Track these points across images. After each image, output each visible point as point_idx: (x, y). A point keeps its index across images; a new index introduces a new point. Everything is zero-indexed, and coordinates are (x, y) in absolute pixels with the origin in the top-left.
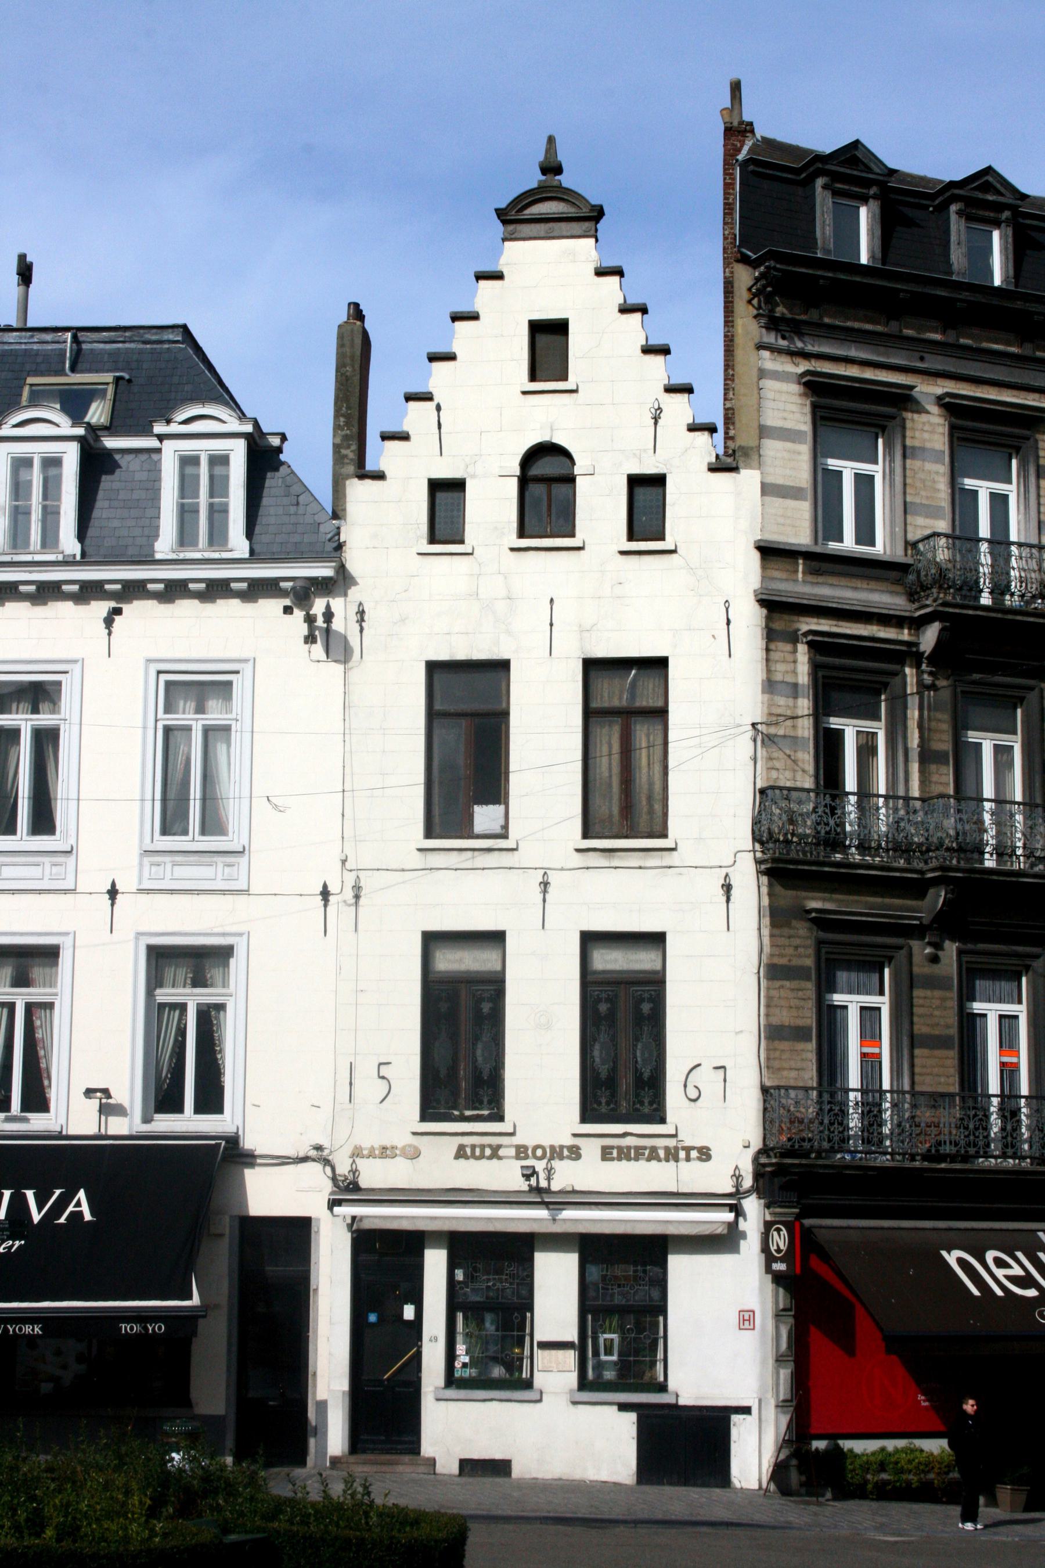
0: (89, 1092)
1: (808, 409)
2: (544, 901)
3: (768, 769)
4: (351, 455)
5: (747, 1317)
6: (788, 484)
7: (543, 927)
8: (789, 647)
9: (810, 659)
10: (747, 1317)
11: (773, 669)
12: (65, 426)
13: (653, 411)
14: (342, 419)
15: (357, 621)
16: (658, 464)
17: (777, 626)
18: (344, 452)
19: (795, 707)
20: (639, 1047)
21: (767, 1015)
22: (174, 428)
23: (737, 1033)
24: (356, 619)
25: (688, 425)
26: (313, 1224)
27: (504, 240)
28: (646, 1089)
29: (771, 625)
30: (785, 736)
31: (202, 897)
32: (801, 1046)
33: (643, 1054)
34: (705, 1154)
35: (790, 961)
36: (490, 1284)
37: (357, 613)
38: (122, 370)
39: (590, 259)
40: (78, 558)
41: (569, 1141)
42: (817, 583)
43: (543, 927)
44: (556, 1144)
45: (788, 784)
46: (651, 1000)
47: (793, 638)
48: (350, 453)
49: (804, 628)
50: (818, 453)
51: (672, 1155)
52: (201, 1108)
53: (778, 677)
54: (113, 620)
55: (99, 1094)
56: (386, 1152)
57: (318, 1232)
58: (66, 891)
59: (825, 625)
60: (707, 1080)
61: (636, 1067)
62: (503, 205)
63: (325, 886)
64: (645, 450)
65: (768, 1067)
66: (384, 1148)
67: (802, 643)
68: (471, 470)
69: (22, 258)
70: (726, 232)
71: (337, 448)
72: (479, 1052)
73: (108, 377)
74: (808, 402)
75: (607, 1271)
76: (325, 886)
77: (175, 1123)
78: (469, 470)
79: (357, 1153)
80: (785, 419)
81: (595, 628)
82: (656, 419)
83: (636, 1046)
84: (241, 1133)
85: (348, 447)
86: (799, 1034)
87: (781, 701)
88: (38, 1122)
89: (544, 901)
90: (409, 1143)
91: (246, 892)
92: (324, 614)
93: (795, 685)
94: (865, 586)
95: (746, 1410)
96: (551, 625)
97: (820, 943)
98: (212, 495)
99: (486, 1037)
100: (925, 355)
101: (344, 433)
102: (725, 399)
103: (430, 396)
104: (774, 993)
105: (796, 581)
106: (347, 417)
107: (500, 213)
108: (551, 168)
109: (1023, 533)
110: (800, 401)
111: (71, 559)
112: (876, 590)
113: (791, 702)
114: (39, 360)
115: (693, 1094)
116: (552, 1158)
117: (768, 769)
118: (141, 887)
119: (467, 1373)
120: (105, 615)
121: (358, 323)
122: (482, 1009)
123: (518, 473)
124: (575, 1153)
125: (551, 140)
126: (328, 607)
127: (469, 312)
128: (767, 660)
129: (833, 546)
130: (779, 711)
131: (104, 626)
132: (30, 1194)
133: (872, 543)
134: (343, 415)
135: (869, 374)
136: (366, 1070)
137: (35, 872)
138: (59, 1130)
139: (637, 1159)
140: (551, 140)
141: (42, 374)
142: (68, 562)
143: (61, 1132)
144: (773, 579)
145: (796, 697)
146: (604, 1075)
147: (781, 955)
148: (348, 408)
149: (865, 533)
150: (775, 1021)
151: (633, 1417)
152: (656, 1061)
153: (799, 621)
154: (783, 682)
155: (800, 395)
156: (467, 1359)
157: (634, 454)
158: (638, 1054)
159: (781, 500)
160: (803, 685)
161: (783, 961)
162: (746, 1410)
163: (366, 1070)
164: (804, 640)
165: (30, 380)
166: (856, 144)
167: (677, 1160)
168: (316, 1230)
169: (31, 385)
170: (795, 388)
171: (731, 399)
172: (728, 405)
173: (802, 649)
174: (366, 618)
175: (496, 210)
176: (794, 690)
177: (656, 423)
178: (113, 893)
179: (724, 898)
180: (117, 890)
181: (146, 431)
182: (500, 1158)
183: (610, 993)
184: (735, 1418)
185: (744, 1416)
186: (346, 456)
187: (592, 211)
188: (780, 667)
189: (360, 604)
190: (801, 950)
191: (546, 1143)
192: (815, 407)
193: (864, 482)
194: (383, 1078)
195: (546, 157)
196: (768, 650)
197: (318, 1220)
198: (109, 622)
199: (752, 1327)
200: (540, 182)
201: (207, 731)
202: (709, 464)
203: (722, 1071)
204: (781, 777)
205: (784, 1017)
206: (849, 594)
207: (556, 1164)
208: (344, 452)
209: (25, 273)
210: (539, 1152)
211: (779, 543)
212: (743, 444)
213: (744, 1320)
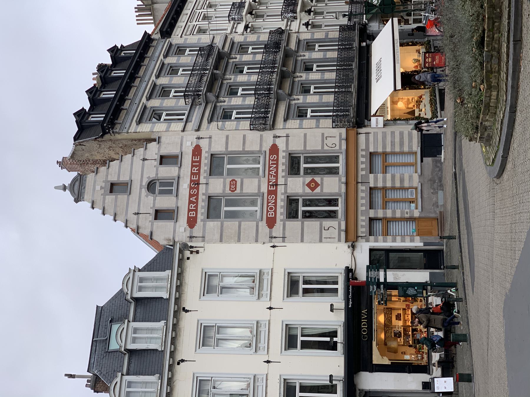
22: (129, 292)
33: (322, 161)
40: (166, 321)
52: (336, 283)
57: (374, 247)
58: (269, 323)
97: (293, 119)
100: (125, 127)
107: (77, 201)
109: (156, 250)
120: (184, 312)
132: (362, 318)
137: (260, 388)
146: (328, 203)
151: (424, 159)
178: (268, 362)
197: (370, 246)
198: (187, 311)
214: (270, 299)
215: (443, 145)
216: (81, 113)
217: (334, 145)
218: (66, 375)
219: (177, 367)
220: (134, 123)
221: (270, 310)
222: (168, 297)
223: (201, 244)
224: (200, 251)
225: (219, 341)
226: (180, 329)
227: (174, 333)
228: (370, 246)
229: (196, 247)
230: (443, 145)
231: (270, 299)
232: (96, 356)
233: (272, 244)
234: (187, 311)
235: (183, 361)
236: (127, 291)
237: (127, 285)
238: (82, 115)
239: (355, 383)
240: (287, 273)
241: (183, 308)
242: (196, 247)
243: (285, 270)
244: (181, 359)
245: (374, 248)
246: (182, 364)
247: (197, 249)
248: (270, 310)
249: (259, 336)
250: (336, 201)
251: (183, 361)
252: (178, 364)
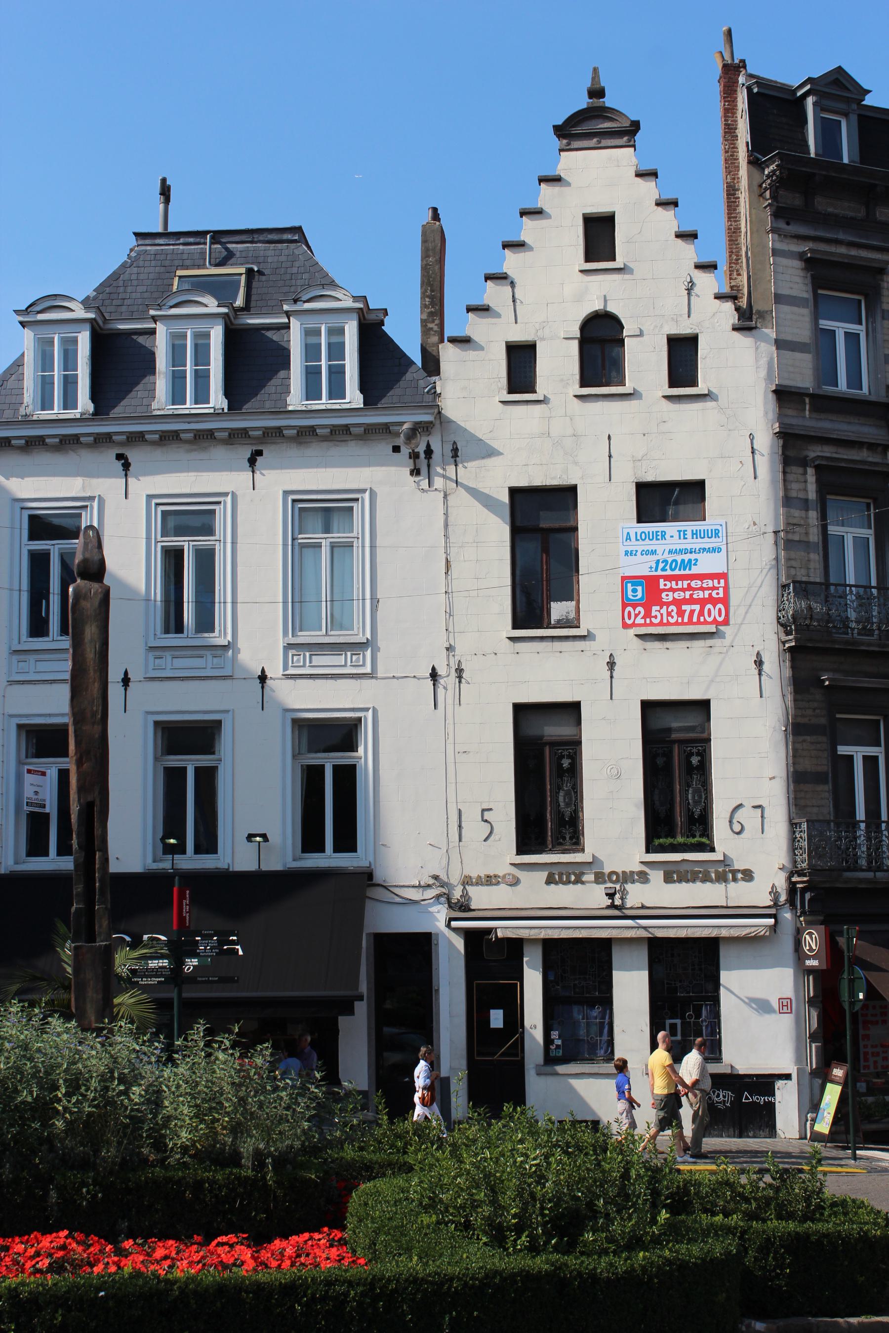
0: (250, 837)
1: (809, 280)
2: (612, 677)
3: (788, 567)
4: (436, 328)
5: (785, 1004)
6: (795, 340)
7: (611, 698)
8: (800, 470)
9: (817, 479)
10: (785, 1004)
11: (789, 487)
12: (211, 305)
13: (686, 283)
14: (427, 300)
15: (452, 457)
16: (691, 326)
17: (791, 453)
18: (430, 325)
19: (807, 518)
20: (690, 792)
21: (794, 764)
23: (771, 779)
24: (451, 455)
25: (715, 294)
26: (433, 937)
27: (561, 150)
28: (697, 825)
29: (788, 453)
30: (799, 541)
31: (55, 686)
32: (820, 788)
33: (693, 797)
34: (748, 875)
35: (810, 720)
36: (577, 982)
37: (452, 450)
38: (252, 263)
39: (631, 164)
40: (226, 410)
41: (638, 868)
42: (821, 419)
43: (611, 698)
44: (628, 870)
45: (804, 579)
46: (698, 754)
47: (804, 463)
48: (433, 326)
49: (812, 455)
50: (816, 316)
51: (721, 878)
53: (793, 494)
54: (256, 460)
55: (258, 839)
56: (490, 880)
57: (437, 945)
59: (827, 451)
60: (747, 817)
61: (689, 808)
62: (560, 123)
63: (434, 669)
64: (681, 315)
65: (796, 805)
66: (488, 877)
67: (810, 467)
68: (540, 333)
69: (164, 180)
70: (727, 147)
71: (424, 323)
72: (561, 799)
73: (243, 270)
74: (809, 275)
75: (670, 970)
76: (434, 669)
77: (319, 860)
78: (539, 334)
79: (467, 881)
80: (791, 288)
81: (644, 458)
82: (689, 290)
83: (688, 791)
84: (373, 867)
85: (433, 322)
86: (819, 778)
87: (797, 513)
88: (207, 862)
89: (612, 677)
90: (509, 872)
92: (425, 452)
93: (806, 501)
94: (856, 421)
95: (788, 1077)
96: (610, 456)
98: (330, 358)
99: (567, 786)
101: (429, 310)
102: (731, 279)
103: (505, 275)
104: (798, 746)
105: (804, 417)
106: (432, 298)
108: (597, 93)
110: (802, 274)
111: (220, 411)
112: (866, 424)
113: (803, 513)
114: (185, 256)
115: (737, 828)
116: (626, 882)
117: (788, 567)
118: (286, 673)
119: (560, 1053)
120: (249, 456)
121: (438, 223)
122: (563, 764)
123: (579, 336)
124: (643, 878)
125: (595, 70)
126: (428, 446)
127: (535, 209)
128: (785, 480)
129: (829, 389)
130: (795, 521)
131: (248, 465)
133: (861, 389)
134: (428, 296)
135: (854, 252)
136: (472, 817)
137: (341, 660)
138: (227, 867)
139: (694, 881)
140: (595, 70)
141: (187, 268)
142: (217, 415)
143: (228, 869)
144: (786, 416)
145: (807, 510)
147: (803, 716)
148: (432, 291)
149: (855, 379)
150: (800, 768)
152: (704, 802)
153: (807, 450)
154: (797, 498)
155: (802, 269)
156: (559, 1042)
157: (672, 318)
158: (690, 797)
159: (790, 353)
160: (812, 500)
161: (805, 720)
162: (788, 1077)
163: (472, 817)
164: (812, 465)
165: (180, 273)
166: (840, 67)
167: (726, 881)
168: (436, 943)
169: (180, 277)
170: (798, 264)
171: (735, 279)
172: (733, 284)
173: (810, 471)
174: (459, 454)
175: (554, 127)
176: (805, 504)
177: (689, 294)
179: (756, 672)
180: (130, 679)
181: (276, 310)
182: (583, 883)
183: (666, 749)
184: (779, 1084)
185: (786, 1081)
186: (432, 329)
187: (631, 125)
188: (795, 486)
189: (455, 443)
190: (818, 711)
191: (619, 870)
192: (813, 278)
193: (852, 339)
194: (486, 821)
195: (592, 84)
196: (784, 473)
198: (252, 462)
199: (789, 1011)
200: (588, 103)
201: (333, 546)
202: (733, 325)
203: (759, 811)
204: (798, 574)
205: (807, 765)
206: (845, 427)
207: (629, 887)
208: (430, 325)
209: (165, 192)
210: (614, 878)
211: (791, 387)
212: (760, 308)
213: (783, 1006)
218: (164, 180)
219: (112, 454)
225: (305, 550)
226: (205, 449)
227: (190, 436)
232: (171, 247)
233: (441, 671)
235: (126, 466)
236: (304, 298)
241: (262, 451)
242: (429, 466)
244: (130, 461)
246: (119, 465)
247: (424, 470)
249: (189, 653)
250: (571, 838)
251: (126, 466)
252: (119, 457)
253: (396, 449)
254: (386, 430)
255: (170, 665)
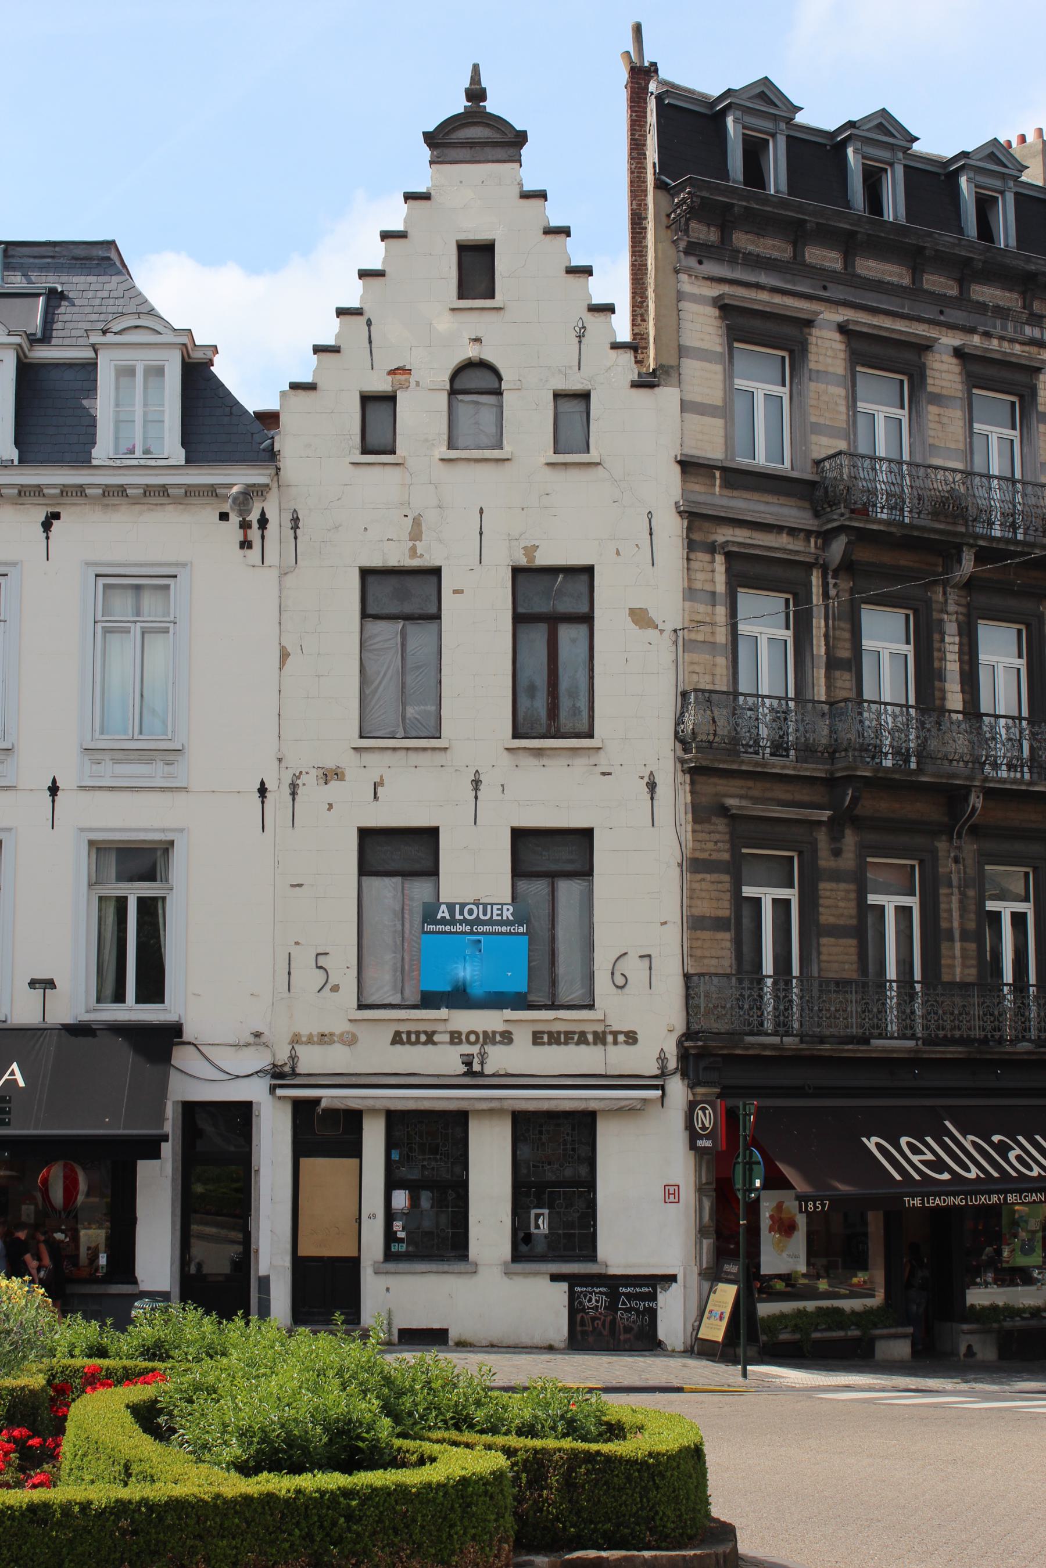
57: (258, 1116)
63: (262, 783)
91: (185, 789)
120: (43, 519)
178: (54, 790)
197: (259, 1104)
198: (47, 526)
214: (82, 788)
215: (745, 1374)
216: (776, 106)
217: (620, 981)
220: (714, 291)
221: (49, 788)
222: (95, 462)
223: (272, 557)
224: (248, 552)
228: (259, 1104)
229: (263, 537)
230: (745, 1374)
231: (82, 788)
234: (47, 526)
237: (137, 327)
238: (772, 111)
239: (688, 1132)
240: (169, 837)
242: (263, 537)
243: (181, 830)
245: (254, 1119)
248: (49, 788)
253: (224, 517)
254: (212, 492)
255: (109, 772)
